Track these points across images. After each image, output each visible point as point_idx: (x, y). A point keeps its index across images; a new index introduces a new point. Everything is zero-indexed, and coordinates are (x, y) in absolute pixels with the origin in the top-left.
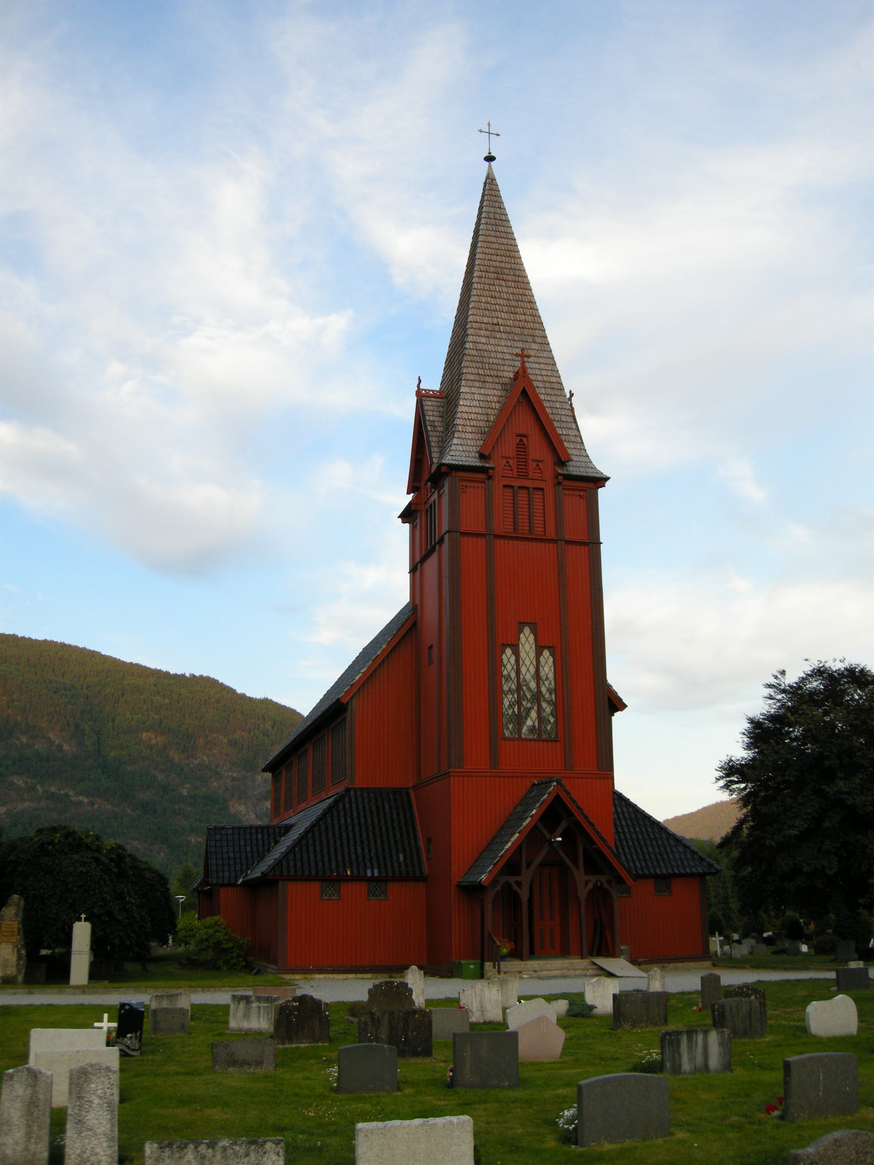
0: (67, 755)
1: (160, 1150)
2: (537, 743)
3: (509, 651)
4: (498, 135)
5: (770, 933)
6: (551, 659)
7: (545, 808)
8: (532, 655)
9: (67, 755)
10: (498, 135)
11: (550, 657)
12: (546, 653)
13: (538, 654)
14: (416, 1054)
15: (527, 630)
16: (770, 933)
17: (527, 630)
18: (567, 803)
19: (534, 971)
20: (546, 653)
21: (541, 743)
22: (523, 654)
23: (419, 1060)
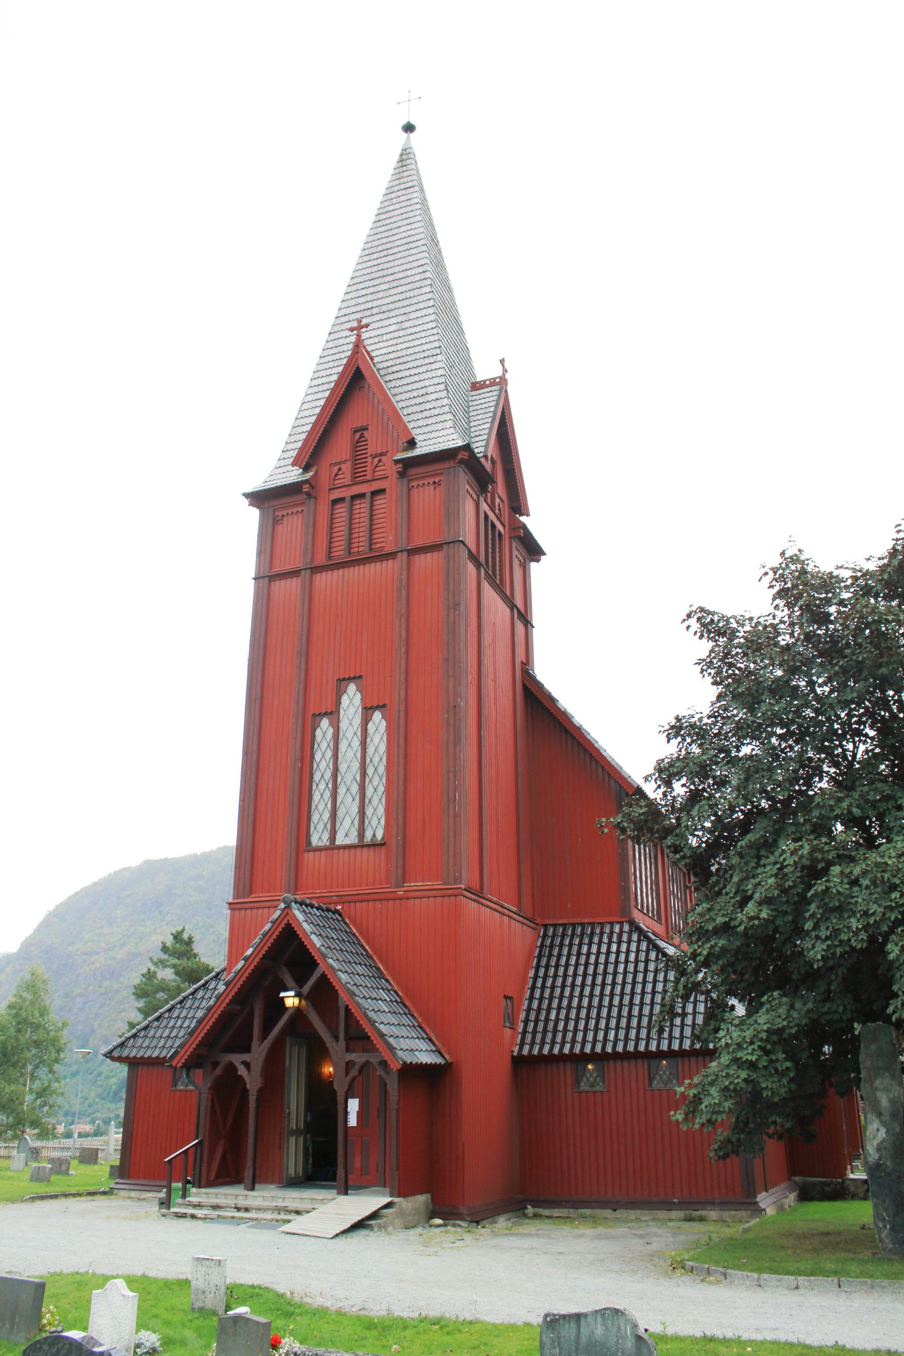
0: (596, 1346)
1: (405, 480)
2: (358, 851)
3: (325, 723)
4: (409, 91)
5: (353, 1121)
6: (384, 723)
7: (315, 972)
8: (358, 721)
9: (596, 1346)
10: (409, 91)
11: (383, 720)
12: (377, 716)
13: (366, 720)
14: (89, 1163)
15: (352, 688)
16: (353, 1121)
17: (352, 688)
18: (242, 983)
19: (236, 1208)
20: (377, 716)
21: (365, 850)
22: (344, 724)
23: (92, 1166)
